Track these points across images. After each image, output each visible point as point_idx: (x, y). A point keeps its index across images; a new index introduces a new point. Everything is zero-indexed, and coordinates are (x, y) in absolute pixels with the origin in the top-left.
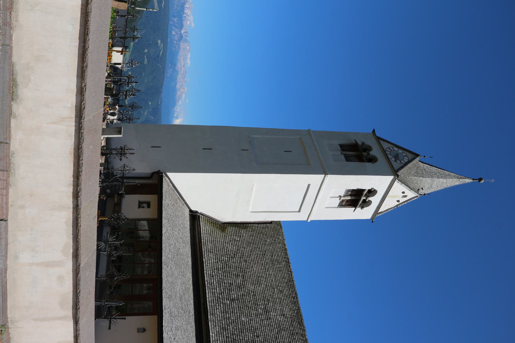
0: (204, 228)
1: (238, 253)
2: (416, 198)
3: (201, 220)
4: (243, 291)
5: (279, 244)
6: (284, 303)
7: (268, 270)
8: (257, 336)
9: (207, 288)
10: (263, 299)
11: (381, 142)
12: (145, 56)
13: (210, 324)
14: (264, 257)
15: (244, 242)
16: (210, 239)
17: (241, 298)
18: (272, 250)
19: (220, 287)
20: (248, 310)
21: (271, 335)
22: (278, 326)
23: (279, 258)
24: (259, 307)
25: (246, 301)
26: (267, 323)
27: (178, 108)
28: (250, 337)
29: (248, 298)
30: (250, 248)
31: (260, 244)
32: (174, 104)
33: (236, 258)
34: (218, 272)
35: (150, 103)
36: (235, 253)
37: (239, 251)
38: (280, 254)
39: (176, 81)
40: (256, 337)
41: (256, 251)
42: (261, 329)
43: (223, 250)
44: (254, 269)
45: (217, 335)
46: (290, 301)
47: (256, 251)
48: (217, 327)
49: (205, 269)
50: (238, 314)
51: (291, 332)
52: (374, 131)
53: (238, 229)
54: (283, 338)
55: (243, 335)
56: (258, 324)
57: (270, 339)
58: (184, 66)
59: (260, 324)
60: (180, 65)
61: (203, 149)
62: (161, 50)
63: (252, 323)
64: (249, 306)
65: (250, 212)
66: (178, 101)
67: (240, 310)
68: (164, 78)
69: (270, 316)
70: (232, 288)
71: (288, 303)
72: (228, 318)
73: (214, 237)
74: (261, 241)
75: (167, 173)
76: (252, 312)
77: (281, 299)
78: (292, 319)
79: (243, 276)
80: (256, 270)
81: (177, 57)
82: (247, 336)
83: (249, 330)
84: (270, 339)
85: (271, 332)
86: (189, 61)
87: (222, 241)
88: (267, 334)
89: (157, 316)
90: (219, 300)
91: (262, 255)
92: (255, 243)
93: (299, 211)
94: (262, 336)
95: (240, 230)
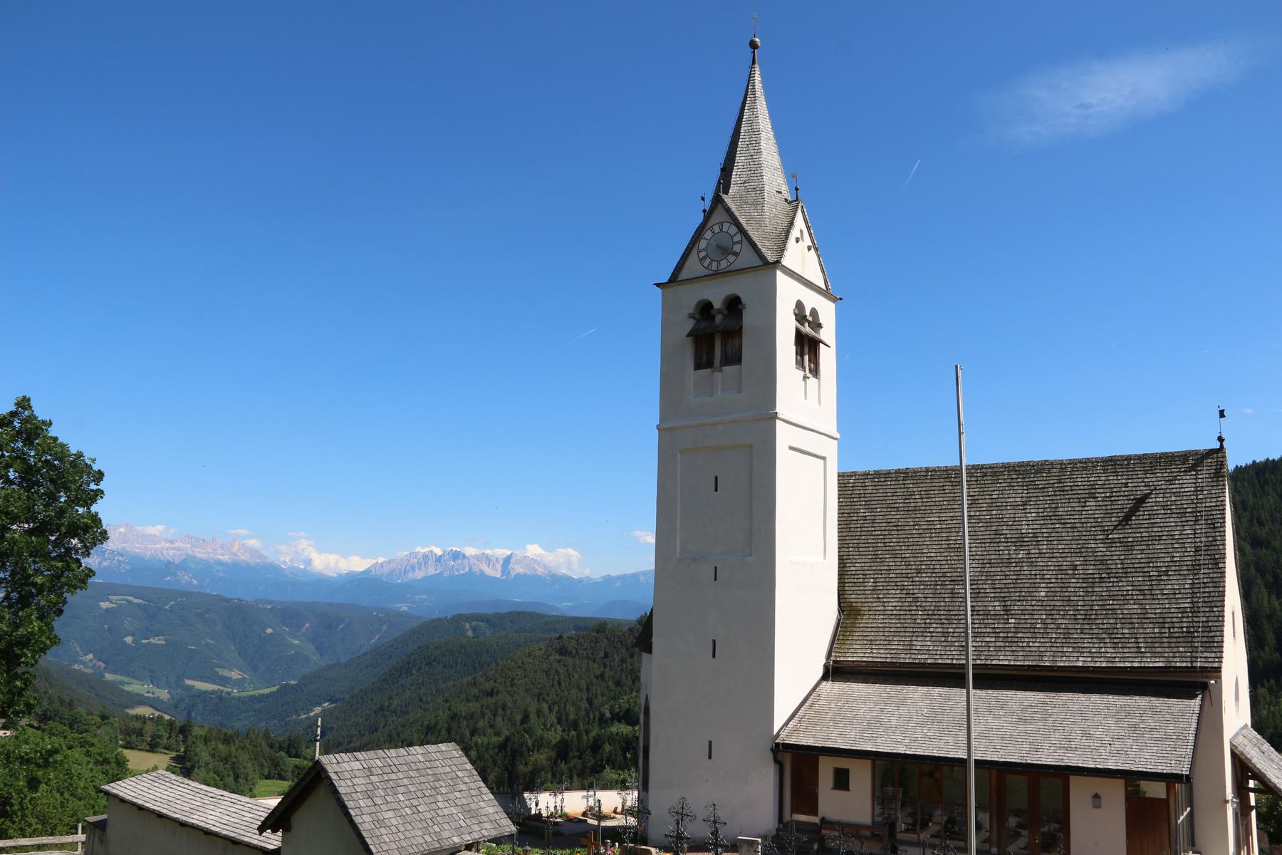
0: (857, 654)
2: (805, 210)
3: (842, 659)
4: (985, 586)
5: (868, 488)
6: (1000, 500)
7: (931, 523)
8: (1073, 570)
9: (989, 662)
10: (995, 545)
11: (684, 275)
12: (144, 641)
13: (1062, 664)
14: (902, 528)
15: (874, 568)
16: (882, 642)
17: (1001, 592)
18: (884, 506)
19: (982, 634)
20: (1024, 581)
21: (1068, 538)
22: (1049, 522)
23: (899, 494)
24: (1014, 556)
25: (1005, 581)
26: (1045, 543)
27: (282, 559)
28: (1078, 585)
29: (999, 577)
30: (887, 556)
31: (874, 533)
32: (274, 568)
33: (916, 591)
34: (951, 634)
35: (269, 631)
36: (905, 592)
37: (899, 584)
38: (891, 491)
39: (212, 562)
40: (1076, 572)
41: (892, 544)
42: (1060, 559)
43: (902, 617)
44: (933, 555)
45: (1081, 652)
46: (993, 485)
47: (892, 544)
48: (1065, 649)
49: (949, 661)
50: (1034, 603)
51: (1058, 493)
52: (658, 285)
53: (846, 577)
54: (1073, 513)
55: (1075, 598)
56: (1050, 563)
57: (1076, 542)
58: (171, 542)
59: (1049, 560)
60: (170, 553)
61: (714, 656)
62: (128, 602)
63: (1048, 577)
64: (1015, 577)
65: (825, 558)
66: (266, 557)
67: (1026, 598)
68: (203, 593)
69: (1030, 535)
70: (981, 608)
71: (997, 490)
72: (1045, 626)
73: (876, 634)
74: (866, 529)
75: (775, 734)
76: (1025, 573)
77: (990, 505)
78: (1030, 487)
79: (952, 581)
80: (934, 551)
81: (147, 559)
82: (1077, 590)
83: (1063, 585)
84: (1076, 542)
85: (1064, 538)
86: (156, 530)
87: (882, 617)
88: (1067, 547)
89: (1071, 777)
90: (1009, 640)
92: (875, 545)
93: (824, 458)
94: (1073, 559)
95: (849, 573)
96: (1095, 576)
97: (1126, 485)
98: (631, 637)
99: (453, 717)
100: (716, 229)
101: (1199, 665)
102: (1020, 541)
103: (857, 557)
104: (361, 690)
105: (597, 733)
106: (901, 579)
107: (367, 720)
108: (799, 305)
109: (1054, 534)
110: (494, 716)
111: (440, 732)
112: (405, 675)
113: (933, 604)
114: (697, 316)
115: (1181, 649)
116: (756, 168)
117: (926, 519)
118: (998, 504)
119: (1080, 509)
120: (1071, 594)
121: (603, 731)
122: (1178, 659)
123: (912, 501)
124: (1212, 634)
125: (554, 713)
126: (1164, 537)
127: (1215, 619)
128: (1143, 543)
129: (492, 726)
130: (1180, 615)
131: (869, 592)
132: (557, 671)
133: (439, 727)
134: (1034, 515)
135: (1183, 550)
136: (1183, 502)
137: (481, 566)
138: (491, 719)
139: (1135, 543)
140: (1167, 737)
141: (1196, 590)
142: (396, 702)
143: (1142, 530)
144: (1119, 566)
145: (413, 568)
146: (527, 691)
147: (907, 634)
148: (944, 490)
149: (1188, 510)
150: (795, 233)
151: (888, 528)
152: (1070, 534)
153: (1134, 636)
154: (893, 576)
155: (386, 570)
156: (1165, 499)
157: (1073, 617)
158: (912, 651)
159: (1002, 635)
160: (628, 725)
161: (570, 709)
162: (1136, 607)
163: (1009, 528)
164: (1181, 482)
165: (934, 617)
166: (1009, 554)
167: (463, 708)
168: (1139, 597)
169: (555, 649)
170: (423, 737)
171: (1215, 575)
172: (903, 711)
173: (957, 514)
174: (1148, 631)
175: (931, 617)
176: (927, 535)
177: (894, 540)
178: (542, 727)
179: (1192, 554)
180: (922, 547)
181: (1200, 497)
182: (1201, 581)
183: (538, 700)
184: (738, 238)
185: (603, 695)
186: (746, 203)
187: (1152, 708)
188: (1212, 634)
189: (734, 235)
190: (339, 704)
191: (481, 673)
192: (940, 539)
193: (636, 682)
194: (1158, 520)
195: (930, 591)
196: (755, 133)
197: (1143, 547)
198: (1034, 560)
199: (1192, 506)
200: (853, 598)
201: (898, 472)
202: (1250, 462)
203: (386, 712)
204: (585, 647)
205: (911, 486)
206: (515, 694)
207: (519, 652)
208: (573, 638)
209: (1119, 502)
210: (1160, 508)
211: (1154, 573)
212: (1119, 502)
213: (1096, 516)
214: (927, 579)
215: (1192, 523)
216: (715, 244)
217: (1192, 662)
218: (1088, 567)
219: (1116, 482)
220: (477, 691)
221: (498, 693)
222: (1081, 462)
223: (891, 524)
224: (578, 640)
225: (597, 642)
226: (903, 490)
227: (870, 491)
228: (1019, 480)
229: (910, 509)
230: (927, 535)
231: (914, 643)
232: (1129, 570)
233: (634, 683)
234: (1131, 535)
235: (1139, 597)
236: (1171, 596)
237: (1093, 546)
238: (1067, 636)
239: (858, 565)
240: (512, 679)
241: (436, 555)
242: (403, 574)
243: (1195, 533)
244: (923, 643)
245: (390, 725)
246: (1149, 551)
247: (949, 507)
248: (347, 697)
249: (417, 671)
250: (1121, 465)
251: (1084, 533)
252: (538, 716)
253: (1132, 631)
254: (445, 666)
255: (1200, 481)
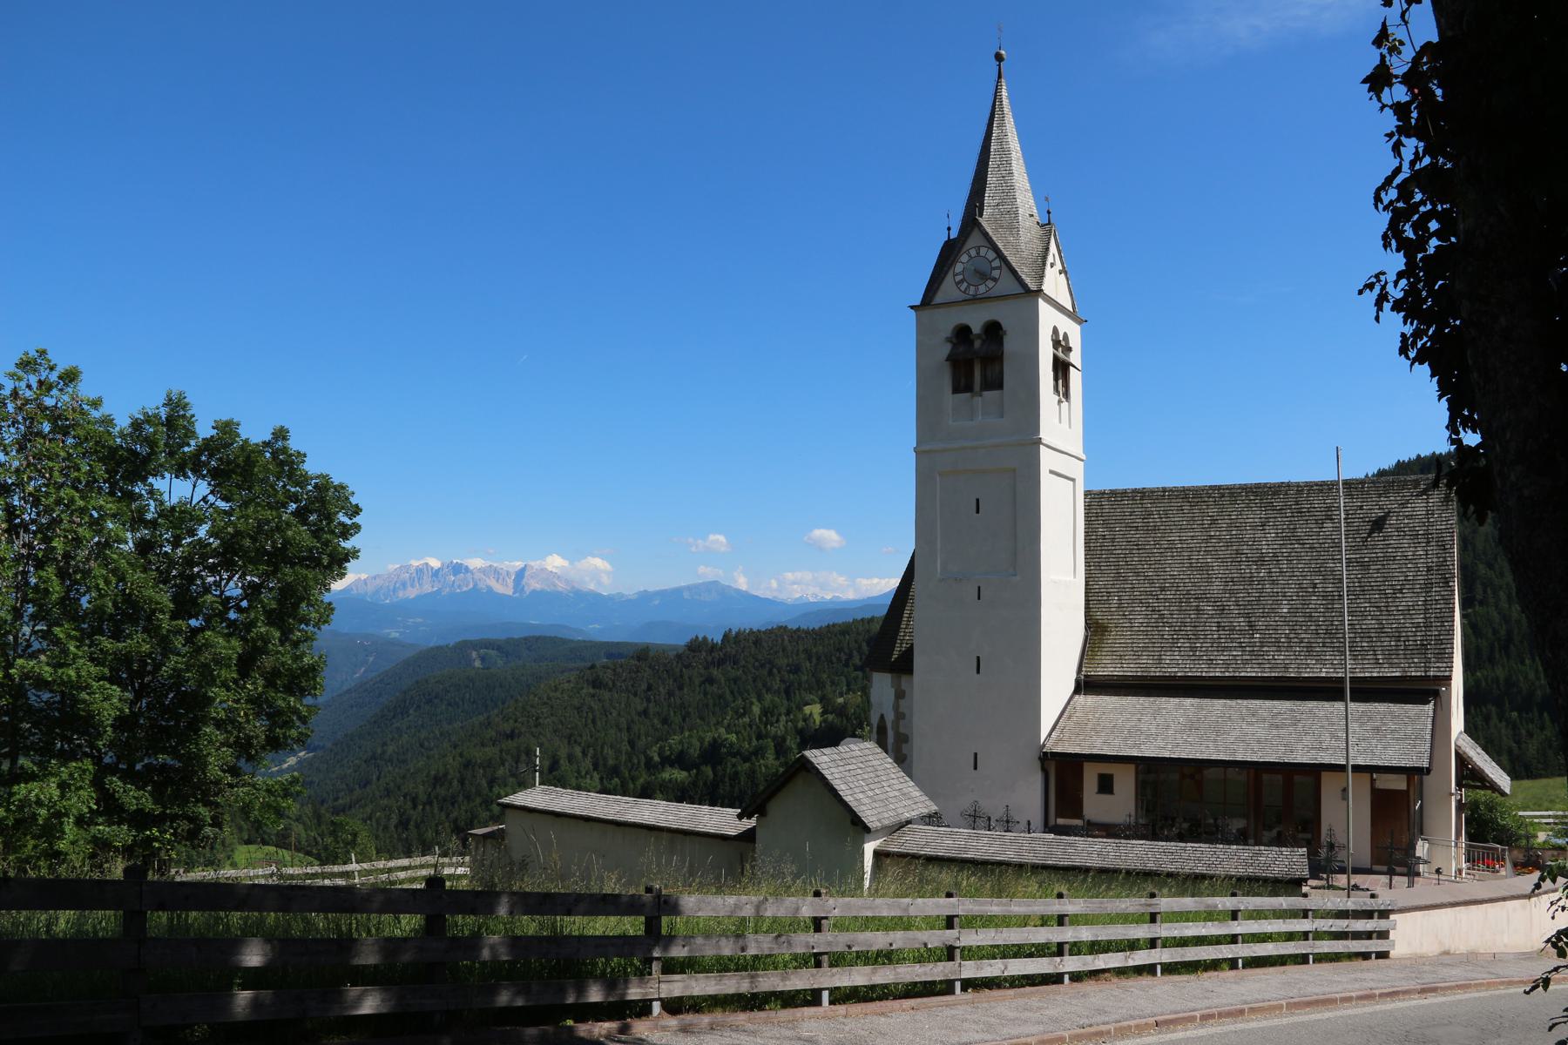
0: (1106, 668)
1: (1149, 603)
6: (1239, 521)
9: (1237, 674)
11: (939, 298)
14: (1143, 547)
15: (1118, 586)
16: (1131, 657)
18: (1123, 525)
20: (1266, 598)
21: (1307, 558)
22: (1288, 542)
24: (1256, 575)
25: (1249, 599)
29: (1242, 595)
31: (1114, 552)
33: (1161, 608)
36: (1150, 609)
37: (1143, 601)
38: (1129, 510)
42: (1300, 578)
44: (1175, 573)
48: (1309, 662)
49: (1199, 674)
51: (1296, 515)
52: (912, 307)
54: (1311, 534)
55: (1316, 614)
56: (1290, 582)
57: (1315, 562)
61: (978, 672)
63: (1290, 594)
65: (1075, 577)
72: (1289, 640)
73: (1125, 649)
76: (1268, 590)
79: (1196, 598)
82: (1317, 606)
87: (1129, 633)
91: (1141, 551)
92: (1117, 564)
93: (1073, 480)
94: (1313, 578)
95: (1093, 591)
96: (1335, 593)
97: (1361, 508)
98: (680, 665)
99: (468, 765)
100: (973, 253)
101: (1432, 674)
102: (1260, 561)
103: (1100, 575)
104: (346, 735)
105: (646, 779)
106: (1146, 597)
107: (355, 771)
108: (1055, 331)
109: (1293, 554)
110: (516, 763)
111: (451, 783)
112: (400, 716)
113: (1179, 620)
114: (954, 340)
115: (1416, 660)
116: (1009, 192)
117: (1166, 539)
118: (1237, 525)
119: (1318, 530)
120: (1312, 610)
121: (653, 777)
122: (1413, 669)
123: (1151, 520)
124: (1444, 646)
125: (589, 758)
126: (1398, 558)
127: (1446, 633)
128: (1379, 563)
129: (513, 775)
130: (1414, 630)
131: (1114, 609)
132: (590, 708)
133: (450, 777)
134: (1273, 535)
135: (1416, 569)
136: (1416, 525)
137: (488, 581)
138: (512, 766)
139: (1371, 563)
140: (1407, 737)
141: (1429, 607)
142: (390, 749)
143: (1377, 551)
144: (1357, 584)
145: (404, 585)
146: (555, 731)
147: (1155, 649)
148: (1182, 510)
149: (1420, 532)
150: (1050, 259)
151: (1128, 547)
152: (1309, 554)
153: (1372, 648)
154: (1138, 593)
155: (370, 588)
156: (1399, 522)
157: (1314, 632)
158: (1162, 665)
159: (1248, 649)
160: (682, 769)
161: (608, 751)
162: (1373, 622)
163: (1249, 547)
164: (1413, 505)
165: (1181, 633)
166: (1251, 573)
167: (478, 754)
168: (1376, 613)
169: (587, 680)
170: (430, 790)
171: (1446, 593)
172: (1159, 720)
173: (1197, 534)
174: (1385, 644)
175: (1178, 633)
176: (1169, 554)
177: (1136, 559)
178: (576, 774)
179: (1424, 573)
180: (1164, 566)
181: (1431, 520)
182: (1433, 598)
183: (569, 742)
184: (996, 263)
185: (647, 735)
186: (1002, 227)
187: (1391, 713)
188: (1444, 646)
189: (992, 261)
190: (320, 753)
191: (496, 711)
192: (1182, 558)
193: (687, 719)
194: (1392, 542)
195: (1175, 608)
196: (1004, 152)
197: (1380, 567)
198: (1275, 578)
199: (1424, 528)
200: (1098, 616)
201: (1135, 491)
202: (1413, 457)
203: (378, 761)
204: (623, 678)
205: (1149, 505)
206: (541, 737)
207: (542, 686)
208: (608, 668)
209: (1355, 524)
210: (1393, 530)
211: (1389, 591)
212: (1355, 524)
213: (1333, 537)
214: (1171, 597)
215: (1424, 545)
216: (973, 268)
217: (1426, 672)
218: (1327, 585)
219: (1351, 504)
220: (494, 733)
221: (519, 735)
222: (1317, 485)
223: (1132, 543)
224: (614, 670)
225: (638, 671)
226: (1140, 510)
227: (1107, 511)
228: (1257, 501)
229: (1150, 528)
230: (1169, 554)
231: (1164, 657)
232: (1366, 588)
233: (684, 720)
234: (1367, 555)
235: (1376, 613)
236: (1406, 612)
237: (1331, 565)
238: (1310, 649)
239: (1101, 583)
240: (537, 719)
241: (432, 568)
242: (392, 593)
243: (1427, 554)
244: (1172, 658)
245: (385, 776)
246: (1384, 571)
247: (1189, 527)
248: (329, 745)
249: (415, 711)
250: (1356, 488)
251: (1322, 553)
252: (569, 762)
253: (1370, 644)
254: (449, 704)
255: (1430, 504)
